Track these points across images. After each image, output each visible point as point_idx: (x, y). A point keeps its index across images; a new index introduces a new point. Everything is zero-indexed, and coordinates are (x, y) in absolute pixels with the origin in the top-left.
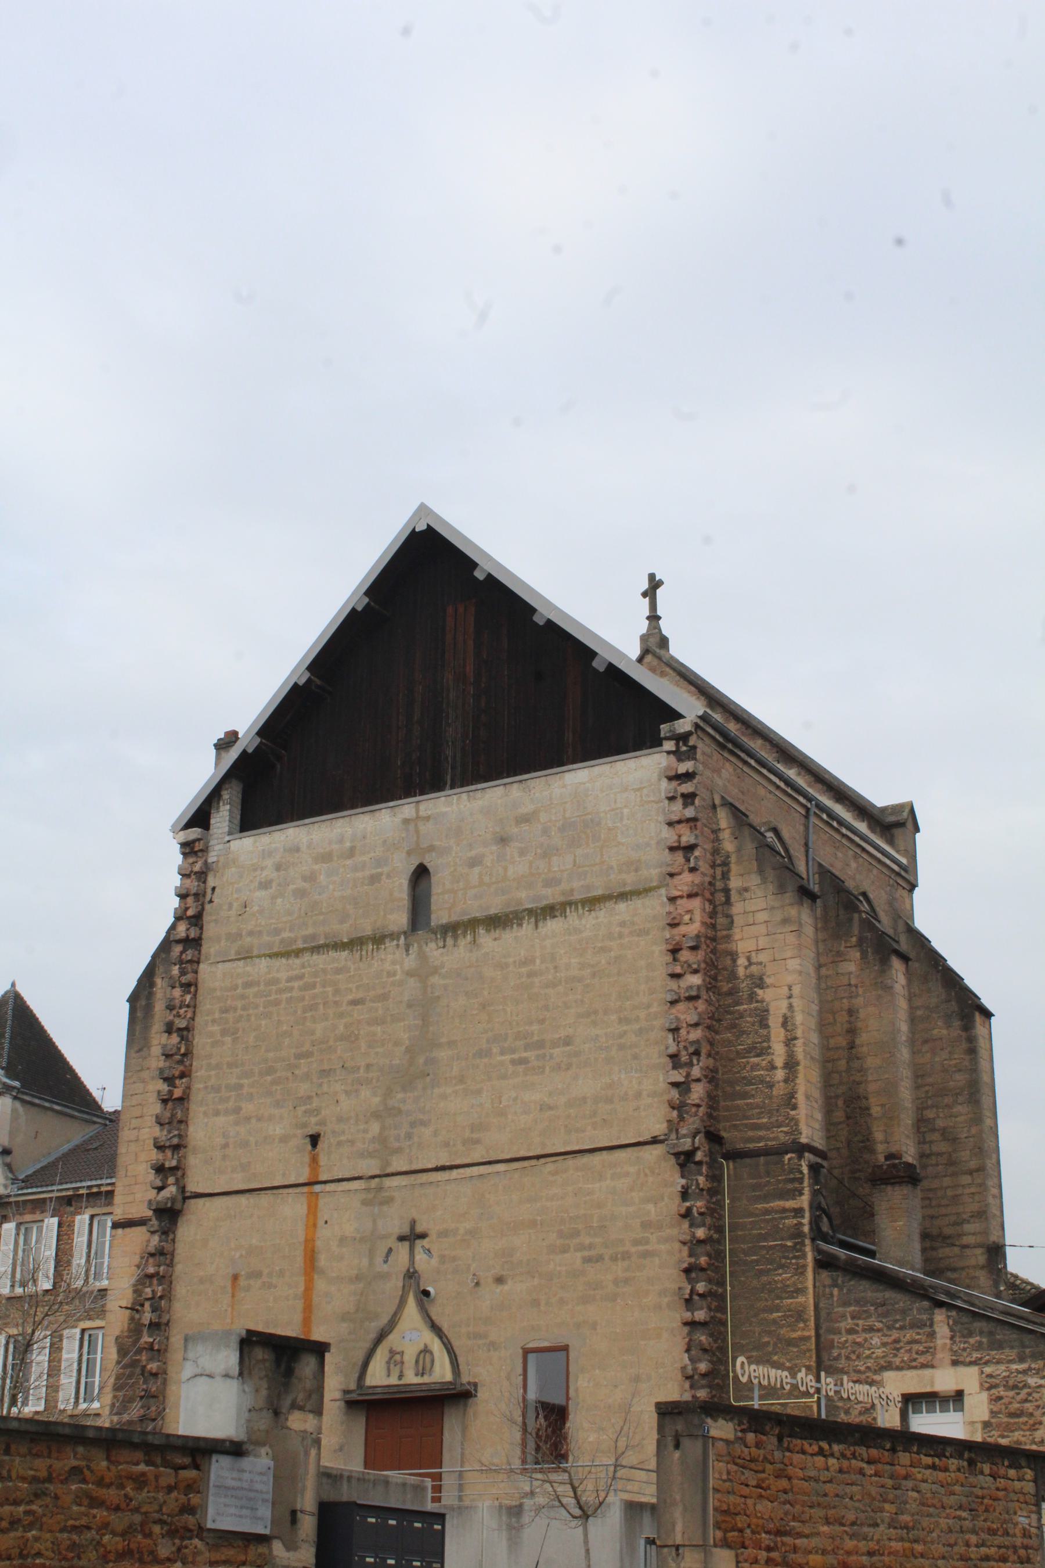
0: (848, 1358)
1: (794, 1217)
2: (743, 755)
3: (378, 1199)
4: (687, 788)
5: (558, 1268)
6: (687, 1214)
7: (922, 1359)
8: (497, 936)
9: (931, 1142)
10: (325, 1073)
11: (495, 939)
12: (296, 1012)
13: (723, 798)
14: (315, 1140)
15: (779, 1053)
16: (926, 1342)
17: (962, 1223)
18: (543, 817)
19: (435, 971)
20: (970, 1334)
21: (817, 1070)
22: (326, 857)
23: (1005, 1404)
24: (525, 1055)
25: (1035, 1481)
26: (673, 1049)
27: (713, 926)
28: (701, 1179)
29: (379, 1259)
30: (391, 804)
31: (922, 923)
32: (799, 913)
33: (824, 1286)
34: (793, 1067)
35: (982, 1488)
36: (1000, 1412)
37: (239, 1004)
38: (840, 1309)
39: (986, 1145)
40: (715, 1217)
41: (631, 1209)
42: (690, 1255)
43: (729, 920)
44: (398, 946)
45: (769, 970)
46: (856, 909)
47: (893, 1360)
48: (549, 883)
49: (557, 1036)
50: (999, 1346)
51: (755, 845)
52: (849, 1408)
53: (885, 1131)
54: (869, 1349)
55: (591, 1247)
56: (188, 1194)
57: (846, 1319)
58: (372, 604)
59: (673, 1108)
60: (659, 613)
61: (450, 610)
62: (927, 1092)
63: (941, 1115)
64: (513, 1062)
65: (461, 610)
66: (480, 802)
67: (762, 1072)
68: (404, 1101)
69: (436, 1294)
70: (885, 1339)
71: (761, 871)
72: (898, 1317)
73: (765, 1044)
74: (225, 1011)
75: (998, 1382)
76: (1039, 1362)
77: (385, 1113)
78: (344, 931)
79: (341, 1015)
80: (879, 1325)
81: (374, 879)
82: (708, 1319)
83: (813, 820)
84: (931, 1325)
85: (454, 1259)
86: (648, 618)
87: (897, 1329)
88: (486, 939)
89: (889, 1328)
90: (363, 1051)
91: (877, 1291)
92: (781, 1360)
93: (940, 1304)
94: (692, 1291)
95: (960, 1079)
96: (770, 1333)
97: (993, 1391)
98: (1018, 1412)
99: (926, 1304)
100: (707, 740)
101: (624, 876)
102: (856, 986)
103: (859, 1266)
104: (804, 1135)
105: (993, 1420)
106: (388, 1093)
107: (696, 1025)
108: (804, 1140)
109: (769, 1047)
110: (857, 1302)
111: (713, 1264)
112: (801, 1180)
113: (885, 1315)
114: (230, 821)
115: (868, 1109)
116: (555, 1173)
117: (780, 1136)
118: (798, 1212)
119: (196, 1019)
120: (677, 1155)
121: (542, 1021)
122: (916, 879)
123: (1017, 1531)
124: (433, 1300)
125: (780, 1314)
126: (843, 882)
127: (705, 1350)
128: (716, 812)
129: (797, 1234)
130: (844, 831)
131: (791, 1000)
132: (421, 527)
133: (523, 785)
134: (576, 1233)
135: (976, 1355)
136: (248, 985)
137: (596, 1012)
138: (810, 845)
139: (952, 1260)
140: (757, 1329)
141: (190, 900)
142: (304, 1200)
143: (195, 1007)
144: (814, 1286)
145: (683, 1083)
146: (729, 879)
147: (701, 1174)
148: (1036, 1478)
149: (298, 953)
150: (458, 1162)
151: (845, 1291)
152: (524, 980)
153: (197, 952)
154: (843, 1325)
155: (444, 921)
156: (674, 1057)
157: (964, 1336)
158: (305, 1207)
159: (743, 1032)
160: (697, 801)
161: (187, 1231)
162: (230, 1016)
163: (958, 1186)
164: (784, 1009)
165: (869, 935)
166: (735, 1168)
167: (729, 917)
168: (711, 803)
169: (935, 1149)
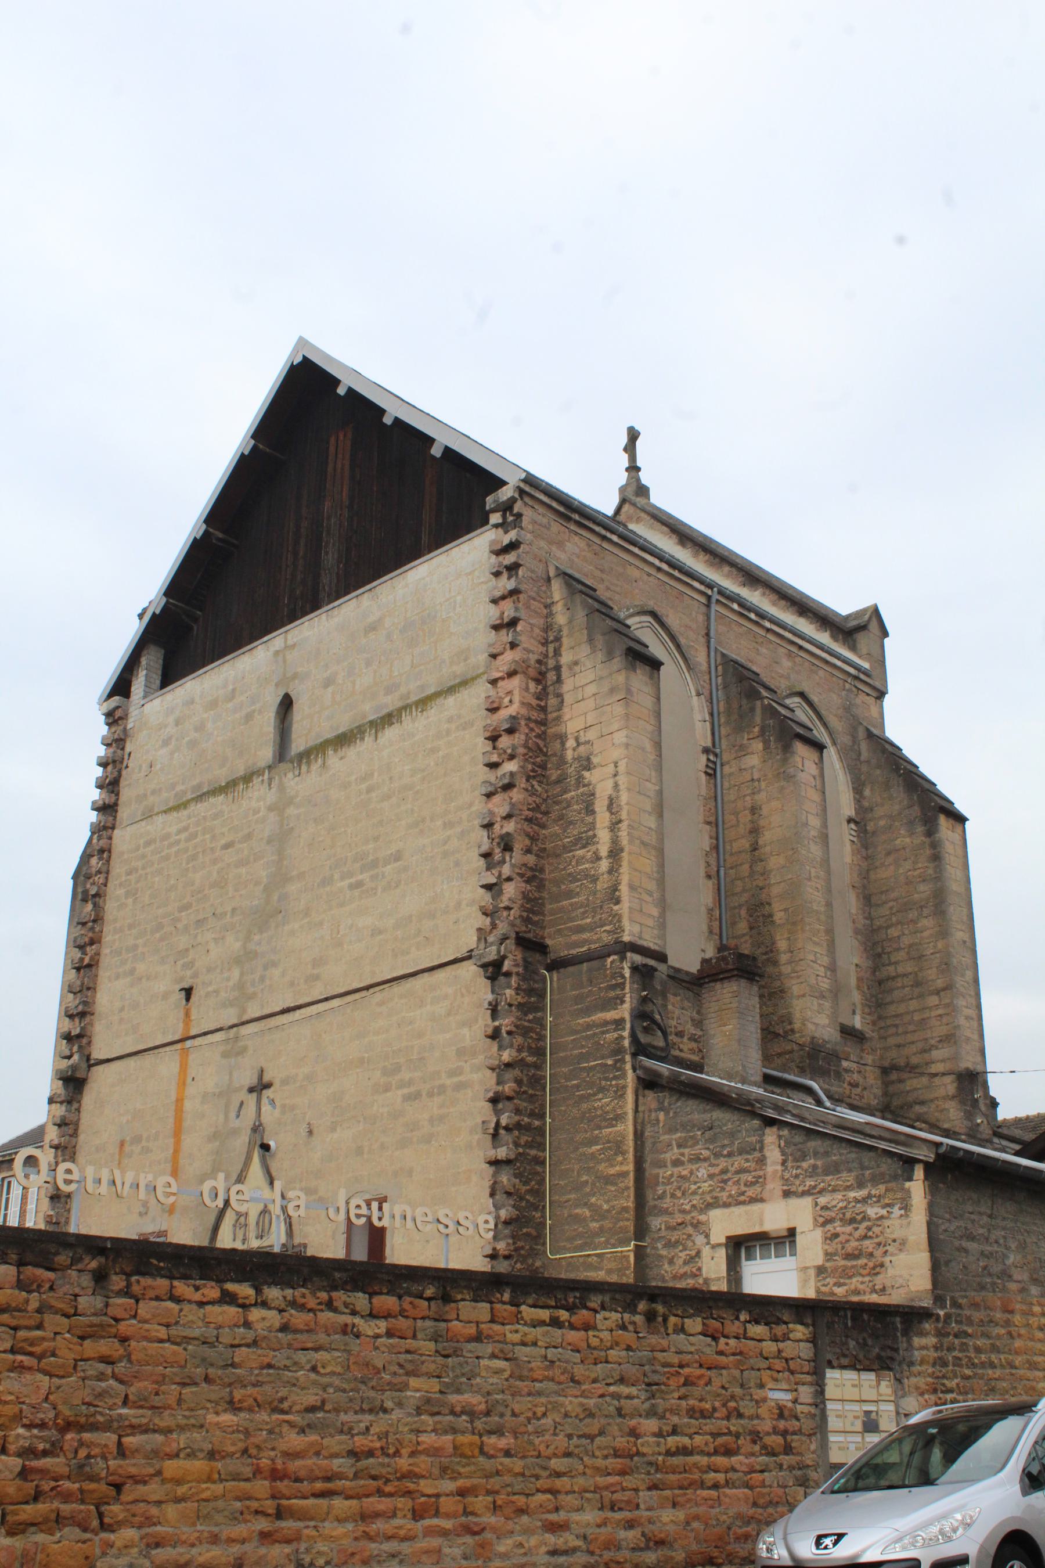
0: (673, 1196)
1: (615, 1030)
2: (597, 529)
3: (235, 1051)
4: (509, 559)
6: (495, 1035)
7: (751, 1192)
8: (343, 754)
9: (896, 963)
10: (200, 923)
11: (341, 758)
13: (557, 568)
14: (188, 992)
16: (755, 1170)
17: (930, 1050)
18: (388, 622)
19: (290, 802)
20: (803, 1157)
21: (652, 858)
22: (213, 704)
23: (841, 1243)
24: (360, 877)
25: (813, 1340)
26: (485, 848)
27: (543, 709)
28: (509, 992)
29: (233, 1115)
30: (265, 639)
31: (893, 732)
32: (627, 678)
33: (650, 1111)
35: (679, 1352)
36: (835, 1254)
37: (140, 864)
38: (666, 1137)
39: (955, 961)
40: (531, 1037)
41: (448, 1036)
42: (498, 1083)
45: (596, 749)
48: (389, 691)
49: (389, 852)
50: (833, 1169)
51: (586, 612)
52: (673, 1257)
53: (789, 939)
54: (695, 1183)
55: (410, 1082)
56: (92, 1062)
57: (672, 1149)
58: (261, 446)
59: (485, 914)
60: (639, 464)
61: (333, 441)
62: (891, 908)
63: (906, 932)
64: (352, 887)
65: (341, 437)
67: (587, 866)
69: (277, 1148)
70: (712, 1170)
71: (591, 640)
72: (726, 1142)
73: (591, 833)
75: (833, 1214)
76: (880, 1186)
77: (244, 958)
78: (222, 775)
79: (215, 862)
80: (706, 1153)
81: (249, 717)
82: (512, 1156)
83: (714, 607)
84: (761, 1149)
85: (293, 1108)
86: (627, 470)
87: (725, 1156)
88: (333, 759)
89: (717, 1155)
90: (230, 895)
91: (705, 1111)
92: (599, 1203)
93: (770, 1122)
94: (498, 1124)
95: (924, 890)
97: (829, 1227)
98: (856, 1252)
99: (756, 1122)
100: (541, 509)
101: (455, 668)
102: (759, 780)
103: (682, 1083)
104: (627, 933)
105: (828, 1265)
106: (248, 938)
108: (626, 938)
109: (595, 836)
110: (684, 1127)
111: (525, 1092)
112: (622, 986)
113: (712, 1140)
114: (146, 686)
115: (771, 916)
116: (381, 1004)
117: (604, 937)
118: (619, 1023)
119: (109, 885)
120: (484, 966)
121: (376, 839)
122: (886, 687)
125: (598, 1147)
128: (550, 585)
129: (619, 1051)
130: (768, 624)
131: (617, 778)
132: (298, 359)
133: (373, 593)
134: (397, 1069)
135: (810, 1182)
136: (148, 843)
139: (920, 1092)
141: (110, 768)
142: (177, 1057)
143: (108, 873)
144: (636, 1111)
145: (495, 884)
146: (560, 655)
147: (509, 987)
148: (814, 1337)
149: (185, 805)
150: (301, 1002)
151: (671, 1115)
152: (362, 797)
153: (111, 818)
154: (669, 1156)
155: (302, 749)
156: (486, 855)
157: (796, 1160)
158: (178, 1065)
159: (571, 823)
160: (520, 572)
162: (133, 877)
163: (924, 1009)
164: (609, 791)
166: (558, 979)
167: (559, 696)
168: (544, 576)
169: (900, 970)
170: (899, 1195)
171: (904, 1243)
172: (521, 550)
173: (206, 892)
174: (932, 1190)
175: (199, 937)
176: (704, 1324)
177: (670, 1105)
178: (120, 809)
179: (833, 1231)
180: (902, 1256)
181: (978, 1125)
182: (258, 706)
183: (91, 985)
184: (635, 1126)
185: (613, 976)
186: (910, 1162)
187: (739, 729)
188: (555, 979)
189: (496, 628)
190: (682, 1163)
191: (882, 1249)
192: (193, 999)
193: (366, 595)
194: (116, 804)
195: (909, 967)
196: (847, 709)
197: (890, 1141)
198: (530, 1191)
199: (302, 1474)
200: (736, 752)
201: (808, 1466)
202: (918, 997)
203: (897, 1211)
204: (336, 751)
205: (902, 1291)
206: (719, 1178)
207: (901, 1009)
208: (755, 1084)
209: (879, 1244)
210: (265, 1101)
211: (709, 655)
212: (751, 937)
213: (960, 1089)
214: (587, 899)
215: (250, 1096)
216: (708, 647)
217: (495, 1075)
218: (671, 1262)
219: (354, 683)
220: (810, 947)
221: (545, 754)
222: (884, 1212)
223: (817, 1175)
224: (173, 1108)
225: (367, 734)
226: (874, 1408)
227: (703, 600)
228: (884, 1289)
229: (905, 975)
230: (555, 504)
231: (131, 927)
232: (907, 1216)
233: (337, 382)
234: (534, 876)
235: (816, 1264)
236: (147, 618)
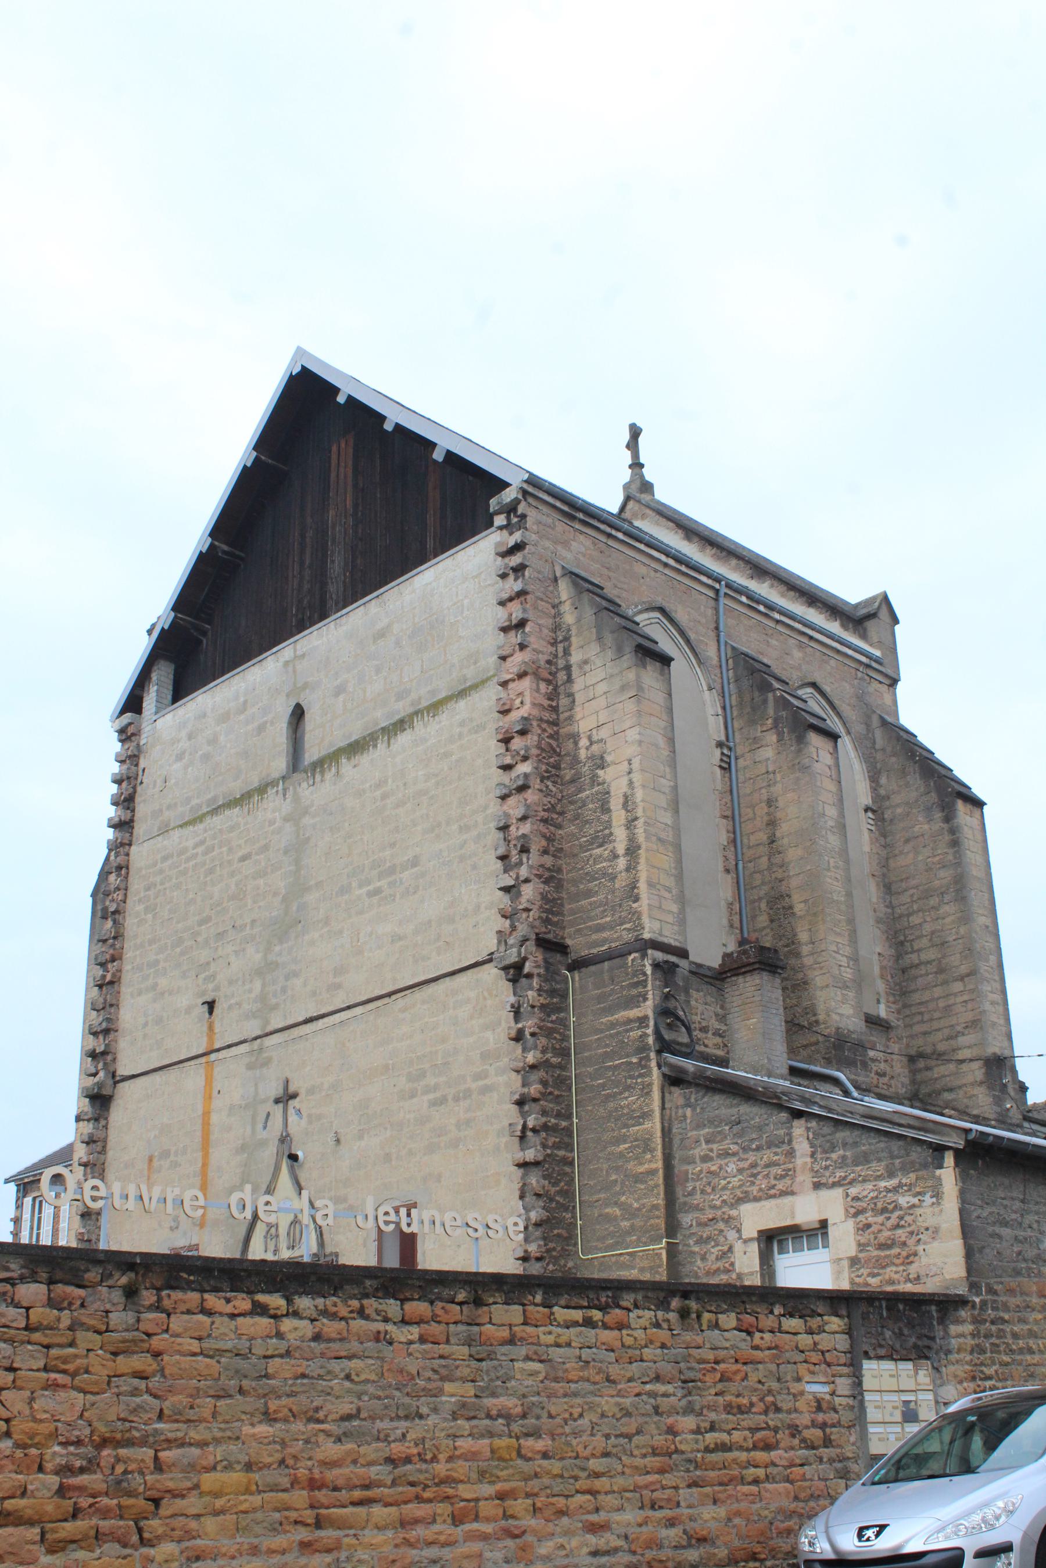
0: (703, 1192)
2: (602, 527)
3: (259, 1063)
4: (515, 560)
5: (407, 1116)
6: (518, 1037)
7: (781, 1185)
9: (919, 950)
11: (355, 766)
12: (199, 878)
14: (211, 1005)
15: (620, 834)
17: (956, 1036)
20: (833, 1148)
21: (670, 854)
23: (874, 1233)
24: (378, 884)
25: (849, 1332)
27: (555, 709)
30: (275, 650)
31: (910, 717)
33: (677, 1108)
34: (634, 852)
36: (868, 1245)
37: (158, 879)
38: (695, 1133)
39: (977, 945)
40: (555, 1038)
41: (471, 1040)
42: (524, 1086)
43: (571, 699)
44: (277, 792)
45: (609, 747)
46: (769, 688)
47: (749, 1189)
48: (399, 697)
49: (406, 858)
50: (864, 1159)
52: (706, 1253)
53: (810, 930)
54: (725, 1179)
55: (436, 1088)
56: (118, 1078)
57: (700, 1145)
59: (504, 916)
60: (642, 461)
61: (334, 449)
62: (912, 896)
63: (928, 919)
65: (343, 445)
66: (345, 628)
68: (280, 954)
69: (305, 1158)
70: (741, 1165)
71: (599, 638)
72: (754, 1136)
73: (607, 832)
74: (148, 889)
75: (865, 1205)
77: (266, 969)
78: (237, 788)
79: (232, 874)
80: (734, 1148)
81: (261, 729)
82: (540, 1158)
83: (723, 600)
84: (790, 1142)
86: (630, 467)
87: (754, 1150)
88: (346, 766)
91: (732, 1106)
93: (798, 1114)
94: (524, 1127)
95: (945, 875)
96: (617, 1169)
97: (861, 1218)
98: (889, 1242)
100: (545, 509)
103: (708, 1078)
104: (647, 930)
105: (861, 1255)
107: (524, 818)
108: (647, 936)
109: (611, 834)
110: (711, 1122)
111: (551, 1093)
114: (157, 701)
115: (791, 907)
116: (403, 1010)
117: (623, 935)
118: (643, 1021)
120: (505, 969)
123: (801, 1404)
124: (301, 1166)
125: (627, 1146)
126: (769, 667)
127: (538, 1195)
128: (557, 584)
129: (644, 1048)
130: (777, 616)
131: (631, 775)
132: (297, 370)
133: (380, 599)
134: (423, 1074)
135: (840, 1173)
136: (165, 859)
137: (439, 825)
138: (721, 628)
139: (948, 1079)
140: (605, 1166)
141: (124, 785)
144: (663, 1108)
145: (513, 886)
146: (570, 655)
147: (531, 988)
148: (850, 1329)
149: (200, 819)
150: (323, 1011)
151: (698, 1110)
152: (378, 803)
153: (128, 835)
155: (315, 758)
156: (503, 858)
157: (825, 1152)
158: (203, 1078)
160: (527, 573)
161: (117, 1115)
162: (151, 893)
164: (625, 789)
165: (784, 713)
166: (580, 979)
167: (571, 695)
169: (924, 956)
170: (930, 1183)
174: (963, 1176)
178: (135, 824)
179: (865, 1221)
181: (1008, 1110)
183: (114, 1002)
184: (662, 1123)
186: (939, 1149)
188: (577, 978)
189: (505, 630)
190: (711, 1159)
191: (914, 1238)
194: (132, 820)
195: (931, 954)
197: (919, 1129)
198: (560, 1192)
200: (750, 744)
201: (849, 1458)
202: (942, 984)
203: (928, 1199)
204: (349, 759)
205: (936, 1279)
206: (749, 1172)
207: (926, 996)
208: (782, 1077)
209: (912, 1233)
210: (291, 1111)
211: (719, 650)
212: (772, 929)
215: (276, 1107)
216: (718, 641)
217: (520, 1077)
218: (704, 1258)
220: (831, 938)
221: (559, 755)
222: (915, 1201)
223: (847, 1165)
225: (380, 741)
226: (913, 1398)
227: (711, 594)
228: (918, 1278)
229: (929, 962)
230: (558, 504)
231: (151, 942)
232: (939, 1204)
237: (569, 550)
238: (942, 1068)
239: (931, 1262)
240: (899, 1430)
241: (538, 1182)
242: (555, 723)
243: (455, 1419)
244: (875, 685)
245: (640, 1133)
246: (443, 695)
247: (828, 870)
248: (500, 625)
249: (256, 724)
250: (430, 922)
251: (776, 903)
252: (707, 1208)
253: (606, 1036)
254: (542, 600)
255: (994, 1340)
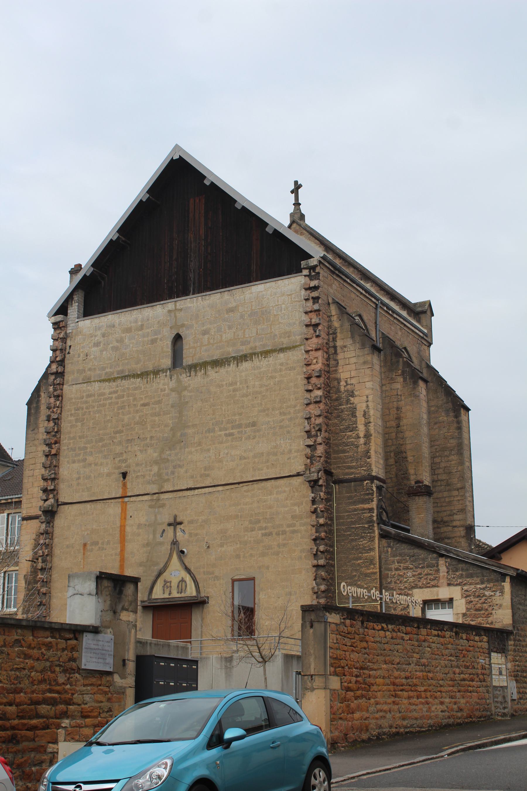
2: (343, 277)
4: (315, 294)
6: (315, 512)
7: (432, 583)
9: (438, 474)
11: (216, 372)
12: (114, 410)
13: (333, 299)
14: (124, 475)
17: (453, 515)
18: (241, 309)
19: (185, 388)
20: (457, 570)
21: (381, 438)
22: (128, 330)
23: (474, 605)
25: (488, 642)
27: (328, 365)
28: (322, 494)
29: (158, 536)
31: (434, 363)
32: (372, 358)
33: (384, 547)
36: (471, 609)
37: (84, 406)
38: (392, 558)
40: (329, 513)
41: (286, 509)
42: (316, 532)
43: (336, 362)
44: (166, 375)
45: (357, 387)
48: (243, 344)
50: (471, 576)
52: (396, 607)
53: (415, 469)
54: (406, 578)
55: (266, 528)
56: (60, 503)
57: (395, 563)
59: (308, 458)
60: (300, 202)
62: (436, 449)
63: (443, 461)
64: (226, 435)
65: (197, 201)
67: (353, 440)
70: (414, 573)
71: (352, 337)
73: (354, 426)
75: (470, 594)
76: (491, 584)
78: (138, 368)
79: (137, 412)
81: (153, 341)
83: (379, 310)
84: (437, 566)
85: (196, 535)
86: (294, 204)
87: (420, 568)
88: (212, 372)
89: (416, 567)
91: (410, 549)
93: (442, 556)
96: (356, 570)
97: (468, 598)
98: (480, 608)
99: (435, 555)
101: (282, 340)
102: (401, 396)
104: (374, 471)
105: (468, 613)
108: (374, 474)
109: (357, 427)
110: (400, 555)
111: (328, 536)
112: (372, 494)
114: (78, 311)
115: (406, 458)
117: (362, 472)
118: (371, 510)
119: (62, 414)
120: (309, 482)
125: (361, 561)
128: (330, 306)
129: (371, 521)
130: (395, 316)
131: (368, 403)
132: (176, 157)
134: (259, 521)
135: (459, 581)
136: (89, 396)
138: (378, 323)
139: (448, 533)
142: (119, 505)
144: (379, 547)
147: (322, 491)
148: (488, 641)
149: (115, 379)
152: (231, 393)
158: (120, 509)
160: (320, 301)
164: (364, 408)
166: (339, 488)
167: (337, 360)
168: (327, 302)
170: (499, 587)
171: (501, 606)
172: (319, 291)
173: (132, 426)
174: (512, 586)
175: (130, 447)
176: (466, 636)
177: (393, 545)
179: (470, 600)
180: (500, 611)
181: (472, 549)
182: (159, 336)
183: (57, 465)
184: (379, 553)
185: (367, 490)
186: (504, 575)
187: (391, 370)
188: (337, 488)
190: (400, 570)
191: (491, 608)
192: (127, 478)
193: (226, 293)
194: (64, 372)
195: (444, 477)
196: (418, 353)
197: (497, 567)
199: (398, 684)
200: (389, 380)
201: (488, 686)
202: (448, 491)
203: (498, 594)
204: (212, 368)
205: (500, 624)
206: (417, 576)
207: (440, 495)
209: (490, 606)
210: (178, 530)
211: (376, 333)
212: (396, 466)
213: (466, 533)
214: (353, 455)
217: (314, 528)
218: (395, 609)
219: (221, 336)
220: (424, 474)
221: (330, 387)
222: (493, 594)
223: (463, 578)
224: (119, 529)
225: (232, 363)
226: (501, 667)
227: (374, 306)
228: (492, 623)
232: (502, 595)
233: (204, 177)
234: (328, 442)
235: (463, 612)
236: (79, 277)
237: (332, 288)
238: (445, 528)
239: (498, 617)
240: (498, 677)
241: (325, 574)
242: (328, 372)
243: (416, 666)
244: (424, 346)
245: (369, 556)
246: (269, 348)
247: (424, 443)
248: (305, 323)
249: (150, 338)
250: (262, 453)
251: (399, 455)
252: (397, 589)
253: (352, 514)
254: (324, 314)
255: (518, 647)
